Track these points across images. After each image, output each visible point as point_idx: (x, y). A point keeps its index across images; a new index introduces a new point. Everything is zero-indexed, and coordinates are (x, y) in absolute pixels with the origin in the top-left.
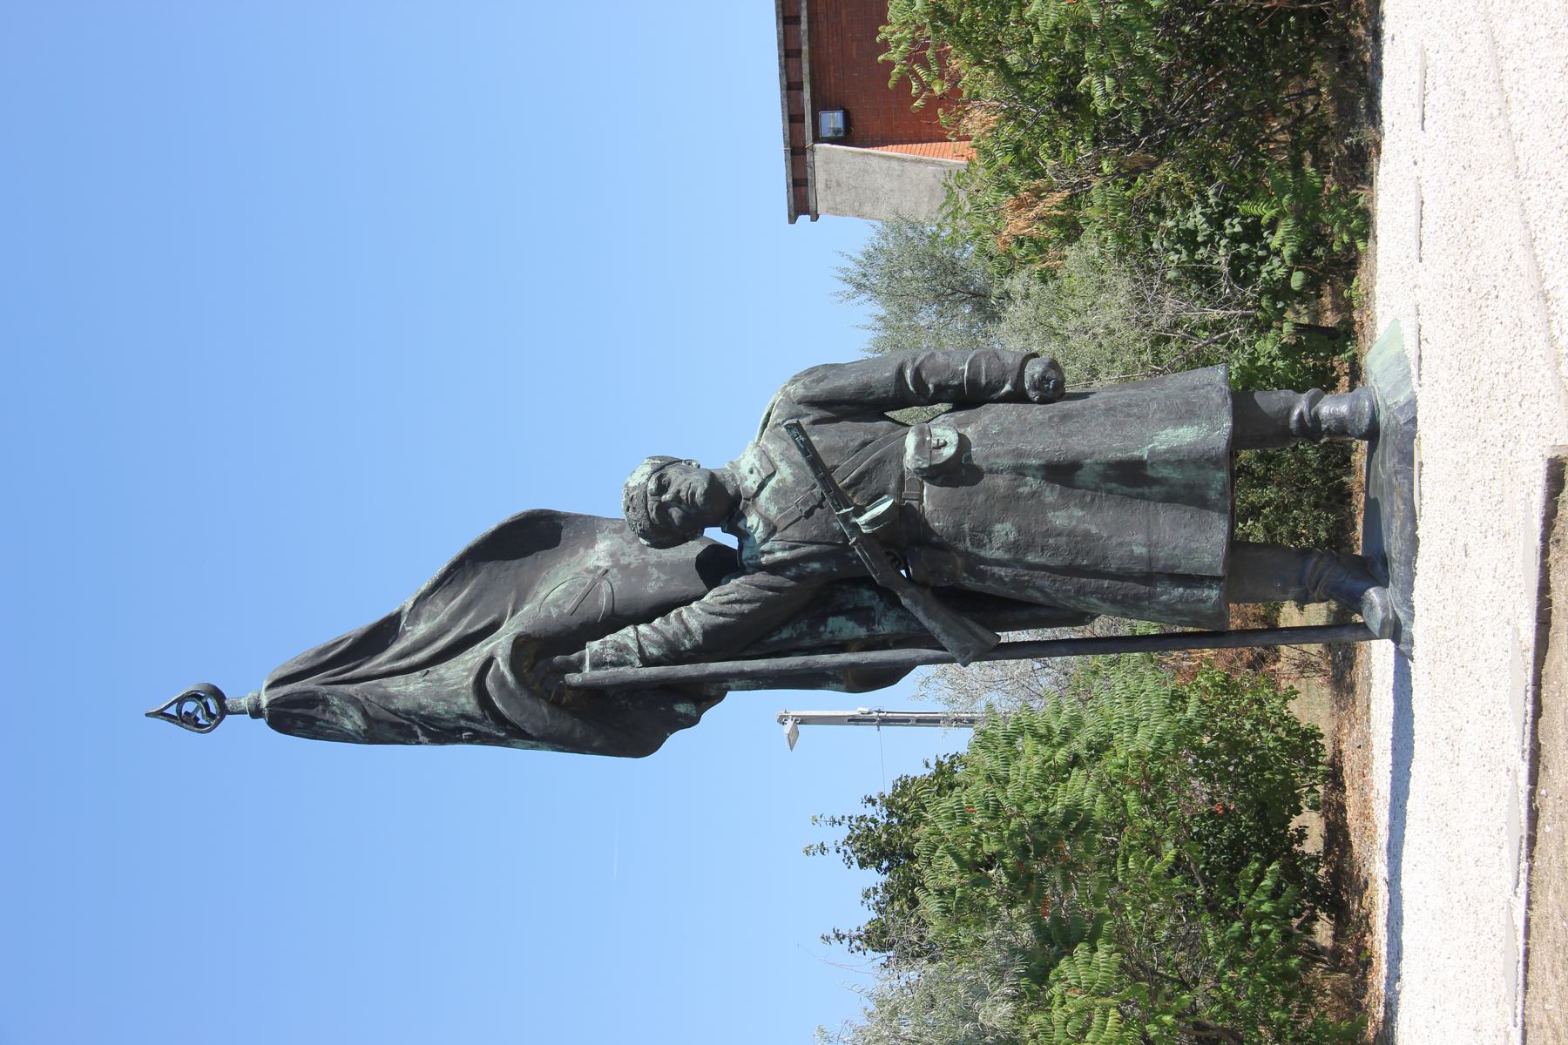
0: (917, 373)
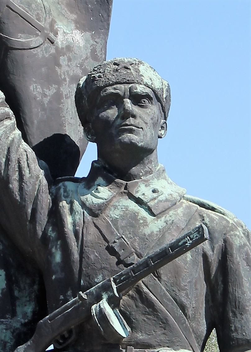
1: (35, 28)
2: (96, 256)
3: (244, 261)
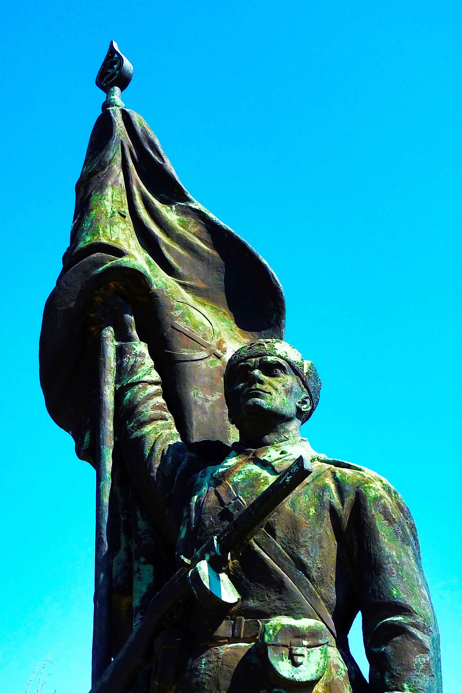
0: (400, 630)
1: (202, 345)
2: (211, 521)
3: (381, 515)
